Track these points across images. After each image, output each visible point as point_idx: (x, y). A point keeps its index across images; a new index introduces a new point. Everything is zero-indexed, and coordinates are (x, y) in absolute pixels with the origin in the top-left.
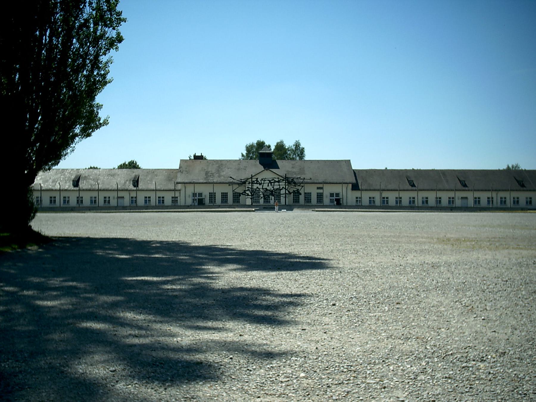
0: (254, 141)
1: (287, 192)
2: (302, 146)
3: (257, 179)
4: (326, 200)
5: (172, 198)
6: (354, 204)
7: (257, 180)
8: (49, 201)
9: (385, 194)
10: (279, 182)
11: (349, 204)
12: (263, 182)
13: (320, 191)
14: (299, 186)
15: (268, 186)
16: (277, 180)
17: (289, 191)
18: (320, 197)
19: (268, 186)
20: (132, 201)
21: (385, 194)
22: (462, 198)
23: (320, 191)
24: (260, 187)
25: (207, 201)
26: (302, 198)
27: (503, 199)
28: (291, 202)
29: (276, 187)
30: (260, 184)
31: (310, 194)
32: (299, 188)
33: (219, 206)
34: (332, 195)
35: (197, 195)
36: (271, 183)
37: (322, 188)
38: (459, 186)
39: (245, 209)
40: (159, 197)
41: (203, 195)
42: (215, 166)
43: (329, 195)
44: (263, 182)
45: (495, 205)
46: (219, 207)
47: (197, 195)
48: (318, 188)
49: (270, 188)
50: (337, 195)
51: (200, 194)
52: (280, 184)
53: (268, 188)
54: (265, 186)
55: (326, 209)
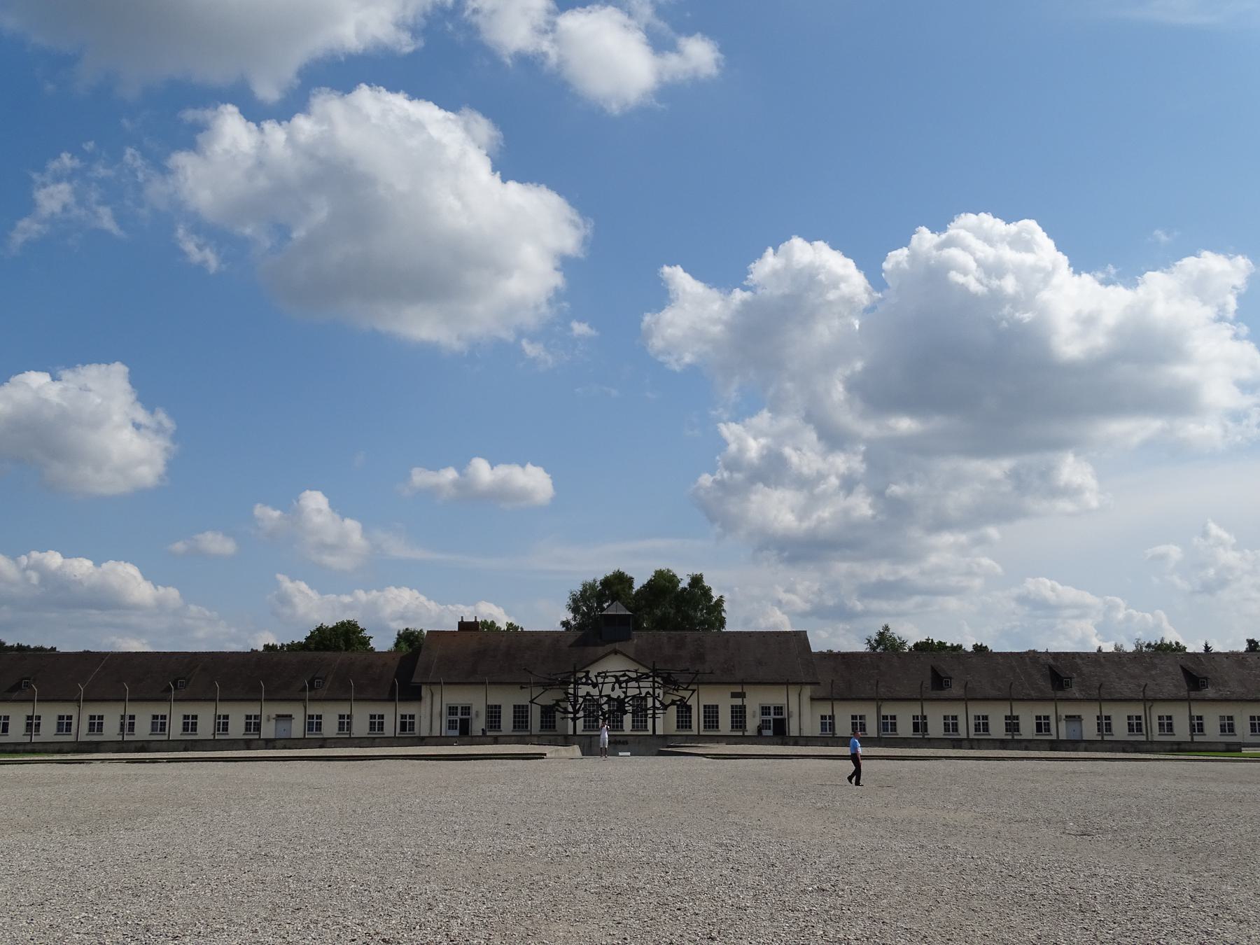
0: (629, 573)
1: (658, 704)
2: (706, 583)
3: (588, 672)
4: (752, 724)
5: (1006, 718)
6: (817, 732)
7: (587, 677)
8: (181, 726)
9: (887, 710)
10: (637, 680)
11: (806, 733)
12: (600, 680)
13: (738, 702)
14: (686, 689)
15: (613, 689)
16: (633, 675)
17: (661, 703)
18: (739, 715)
19: (613, 689)
20: (885, 724)
21: (887, 710)
22: (278, 716)
23: (738, 702)
24: (595, 692)
25: (478, 725)
26: (697, 718)
27: (1166, 722)
28: (673, 729)
29: (631, 692)
30: (595, 685)
31: (466, 710)
32: (686, 694)
33: (1002, 741)
34: (765, 710)
35: (772, 711)
36: (620, 683)
37: (742, 695)
38: (1045, 686)
39: (1156, 756)
40: (403, 717)
41: (473, 711)
42: (404, 646)
43: (758, 712)
44: (600, 680)
45: (962, 734)
46: (507, 740)
47: (772, 711)
48: (734, 695)
49: (618, 693)
50: (779, 710)
51: (466, 710)
52: (642, 684)
53: (614, 695)
54: (607, 690)
55: (1099, 755)
